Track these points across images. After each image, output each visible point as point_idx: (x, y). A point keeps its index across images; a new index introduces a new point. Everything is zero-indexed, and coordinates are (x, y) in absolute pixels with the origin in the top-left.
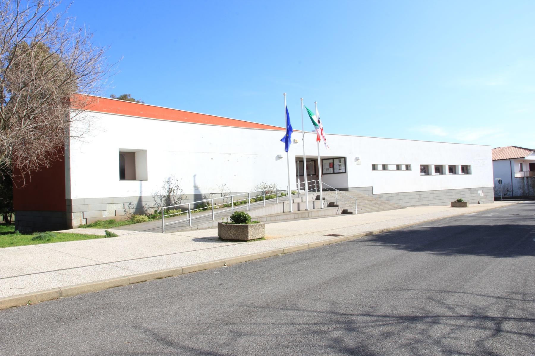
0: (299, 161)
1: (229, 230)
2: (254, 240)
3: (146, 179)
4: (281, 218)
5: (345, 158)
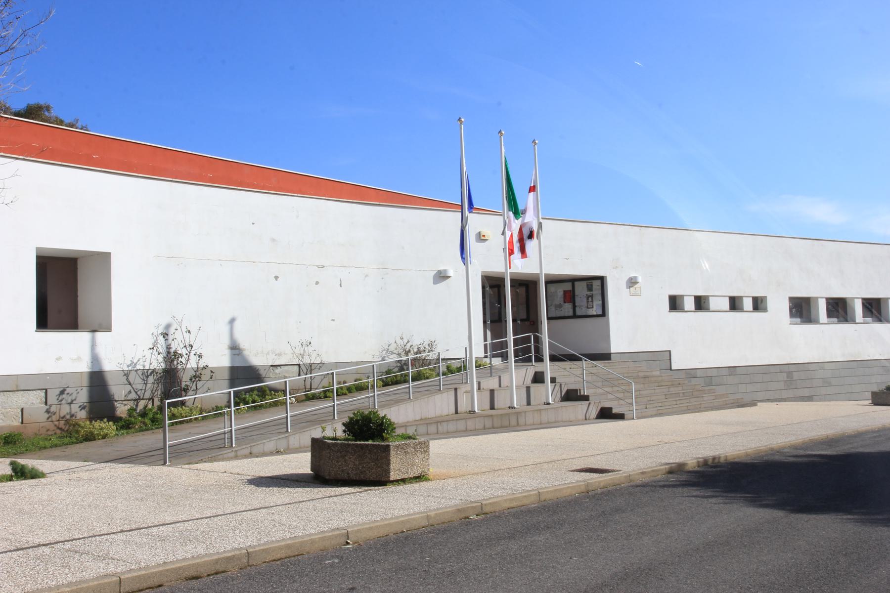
0: (493, 286)
1: (343, 457)
2: (404, 481)
3: (108, 328)
4: (451, 427)
5: (602, 279)
